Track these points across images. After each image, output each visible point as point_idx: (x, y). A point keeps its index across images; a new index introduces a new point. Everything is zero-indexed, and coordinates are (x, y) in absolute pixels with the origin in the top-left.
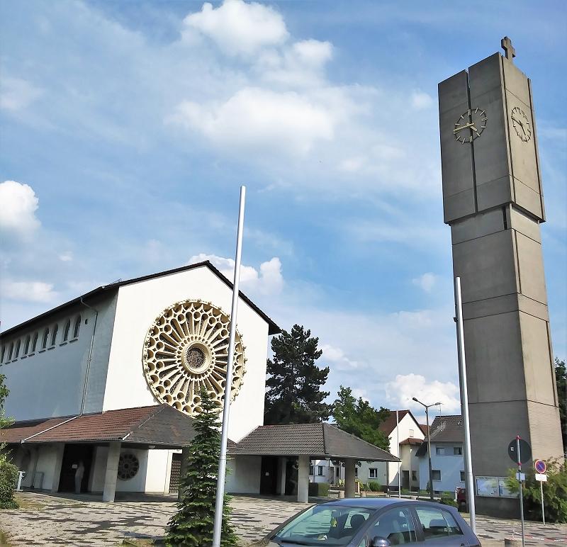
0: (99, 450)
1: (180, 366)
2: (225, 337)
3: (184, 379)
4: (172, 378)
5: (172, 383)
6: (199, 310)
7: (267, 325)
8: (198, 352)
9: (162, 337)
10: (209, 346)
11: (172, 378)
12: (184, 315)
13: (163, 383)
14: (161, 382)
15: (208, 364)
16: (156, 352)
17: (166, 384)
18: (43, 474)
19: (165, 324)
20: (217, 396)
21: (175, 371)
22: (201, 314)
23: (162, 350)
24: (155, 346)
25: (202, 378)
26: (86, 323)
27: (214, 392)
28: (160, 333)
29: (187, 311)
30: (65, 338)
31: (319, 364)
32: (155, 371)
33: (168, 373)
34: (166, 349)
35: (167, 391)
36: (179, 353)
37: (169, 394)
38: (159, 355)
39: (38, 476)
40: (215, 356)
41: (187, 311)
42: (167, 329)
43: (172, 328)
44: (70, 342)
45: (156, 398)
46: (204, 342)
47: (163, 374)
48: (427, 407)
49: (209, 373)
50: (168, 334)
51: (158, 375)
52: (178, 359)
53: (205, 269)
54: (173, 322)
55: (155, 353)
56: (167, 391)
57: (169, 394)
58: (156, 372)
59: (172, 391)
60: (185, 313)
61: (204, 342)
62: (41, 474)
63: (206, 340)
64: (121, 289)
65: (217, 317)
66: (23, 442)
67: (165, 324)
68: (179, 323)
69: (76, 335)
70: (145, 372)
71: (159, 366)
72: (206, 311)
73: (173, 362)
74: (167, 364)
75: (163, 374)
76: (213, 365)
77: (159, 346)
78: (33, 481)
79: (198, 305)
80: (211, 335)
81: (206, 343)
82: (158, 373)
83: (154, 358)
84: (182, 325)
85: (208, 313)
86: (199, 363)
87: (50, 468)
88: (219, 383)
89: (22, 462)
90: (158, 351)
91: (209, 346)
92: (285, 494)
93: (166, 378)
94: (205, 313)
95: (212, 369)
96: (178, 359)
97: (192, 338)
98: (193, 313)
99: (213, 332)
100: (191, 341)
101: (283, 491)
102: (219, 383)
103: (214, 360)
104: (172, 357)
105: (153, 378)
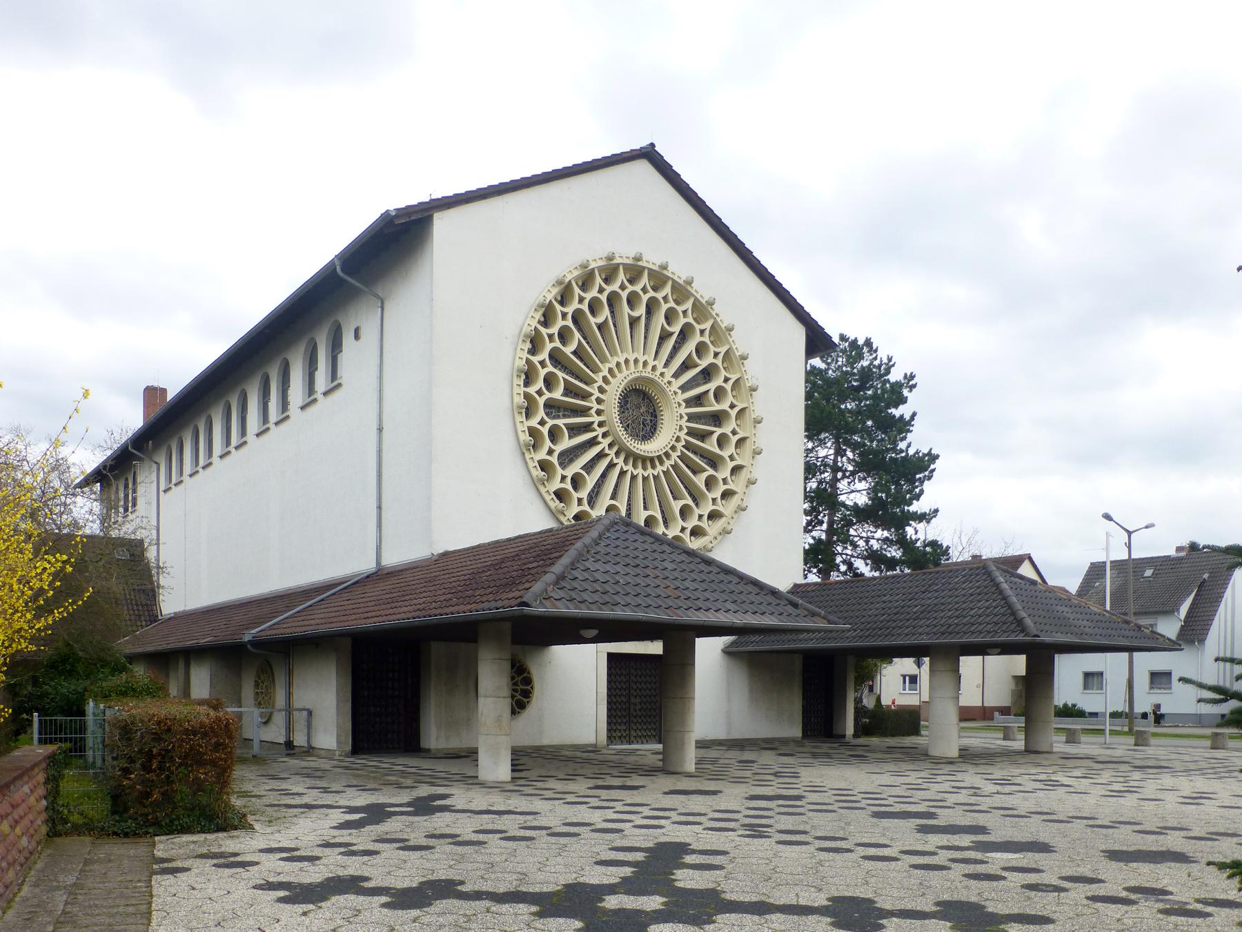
0: (437, 650)
1: (605, 435)
2: (704, 363)
3: (616, 471)
4: (589, 467)
5: (591, 481)
6: (638, 288)
7: (798, 335)
8: (641, 406)
9: (556, 358)
10: (662, 374)
11: (589, 467)
12: (604, 298)
13: (569, 480)
14: (563, 478)
15: (670, 433)
16: (544, 398)
17: (577, 482)
18: (310, 713)
19: (560, 323)
20: (697, 512)
21: (594, 451)
22: (645, 298)
23: (558, 394)
24: (540, 384)
25: (659, 469)
26: (357, 337)
27: (690, 502)
28: (549, 346)
29: (609, 289)
30: (311, 389)
31: (916, 442)
32: (546, 449)
33: (577, 456)
34: (569, 390)
35: (580, 501)
36: (599, 401)
37: (586, 507)
38: (551, 406)
39: (300, 718)
40: (684, 410)
41: (609, 289)
42: (564, 336)
43: (577, 335)
44: (325, 394)
45: (554, 514)
46: (649, 368)
47: (568, 457)
48: (1129, 533)
49: (674, 455)
50: (568, 350)
51: (554, 459)
52: (600, 431)
53: (643, 167)
54: (577, 318)
55: (541, 401)
56: (580, 501)
57: (586, 507)
58: (550, 452)
59: (593, 499)
60: (606, 294)
61: (649, 368)
62: (305, 713)
63: (651, 363)
64: (442, 224)
65: (683, 308)
66: (247, 638)
67: (560, 323)
68: (593, 321)
69: (334, 374)
70: (537, 484)
71: (577, 482)
72: (655, 289)
73: (587, 427)
74: (574, 430)
75: (568, 457)
76: (683, 435)
77: (549, 382)
78: (289, 728)
79: (635, 272)
80: (675, 350)
81: (654, 368)
82: (556, 454)
83: (541, 413)
84: (600, 327)
85: (659, 296)
86: (647, 429)
87: (321, 702)
88: (700, 480)
89: (257, 685)
90: (547, 395)
91: (662, 374)
92: (856, 736)
93: (576, 467)
94: (651, 294)
95: (679, 446)
96: (600, 431)
97: (627, 361)
98: (624, 295)
99: (675, 350)
100: (625, 372)
101: (850, 729)
102: (700, 480)
103: (684, 423)
104: (584, 411)
105: (560, 495)
